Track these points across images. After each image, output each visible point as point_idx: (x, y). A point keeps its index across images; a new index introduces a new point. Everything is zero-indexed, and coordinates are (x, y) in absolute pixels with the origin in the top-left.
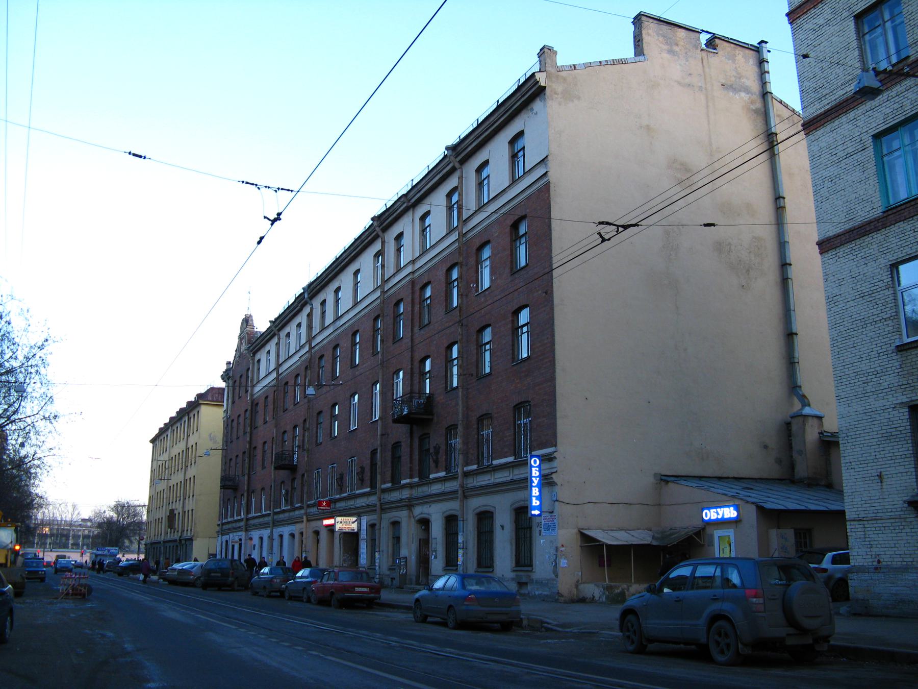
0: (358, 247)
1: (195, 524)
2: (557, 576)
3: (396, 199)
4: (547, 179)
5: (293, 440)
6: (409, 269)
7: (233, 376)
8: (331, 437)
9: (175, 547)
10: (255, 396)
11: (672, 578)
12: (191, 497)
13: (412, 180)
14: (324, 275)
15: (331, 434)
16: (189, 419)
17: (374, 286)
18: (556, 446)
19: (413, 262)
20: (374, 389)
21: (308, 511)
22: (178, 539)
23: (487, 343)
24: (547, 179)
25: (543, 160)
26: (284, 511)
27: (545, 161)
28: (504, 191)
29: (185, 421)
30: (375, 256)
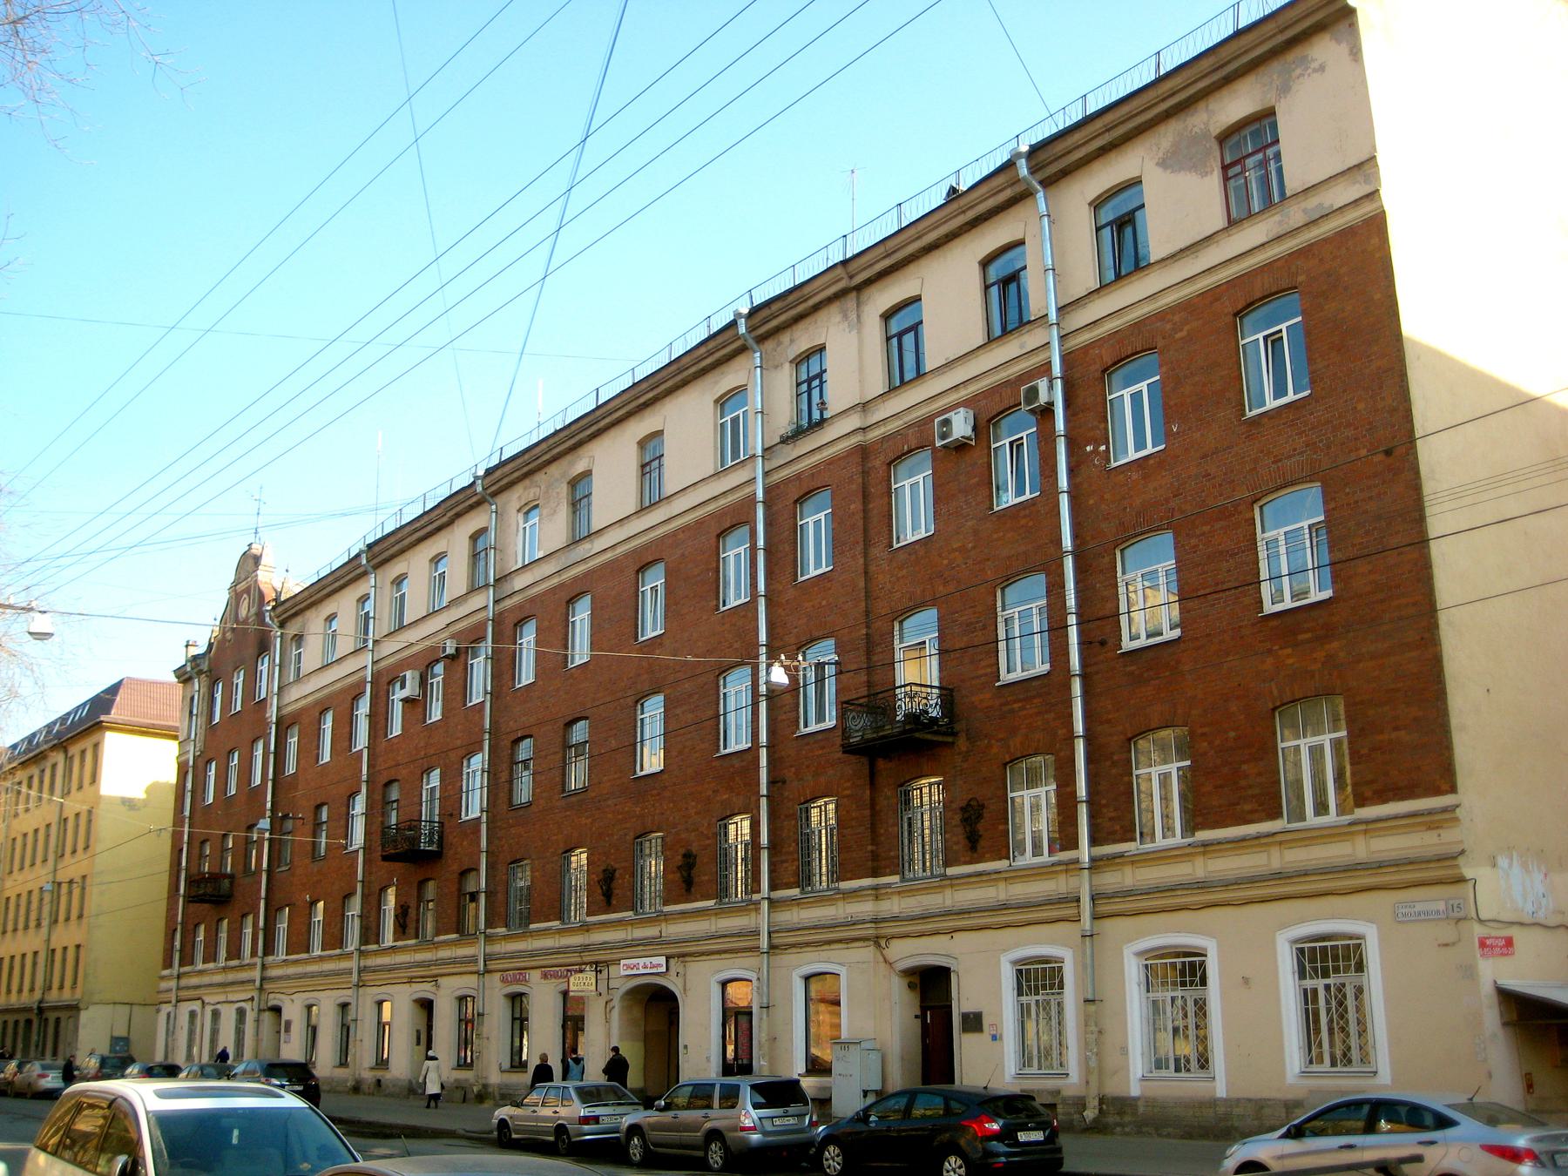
0: (1173, 94)
1: (86, 976)
2: (386, 1096)
3: (1076, 115)
4: (1047, 355)
5: (222, 857)
6: (853, 422)
7: (210, 671)
8: (564, 791)
9: (22, 1025)
10: (289, 709)
11: (764, 1098)
12: (45, 923)
13: (1159, 53)
14: (544, 446)
15: (564, 783)
16: (69, 760)
17: (428, 609)
18: (1453, 789)
19: (864, 406)
20: (465, 764)
21: (362, 964)
22: (35, 1006)
23: (394, 801)
24: (1047, 355)
25: (1359, 166)
26: (201, 972)
27: (1366, 167)
28: (1208, 240)
29: (54, 766)
30: (358, 601)
